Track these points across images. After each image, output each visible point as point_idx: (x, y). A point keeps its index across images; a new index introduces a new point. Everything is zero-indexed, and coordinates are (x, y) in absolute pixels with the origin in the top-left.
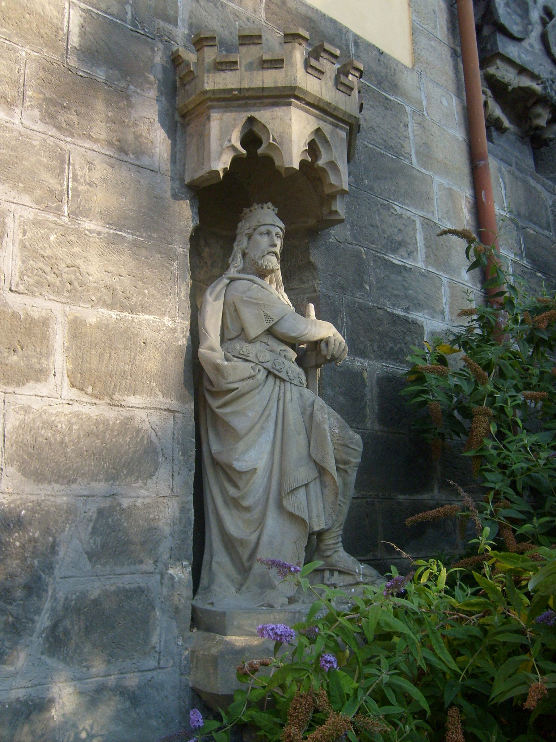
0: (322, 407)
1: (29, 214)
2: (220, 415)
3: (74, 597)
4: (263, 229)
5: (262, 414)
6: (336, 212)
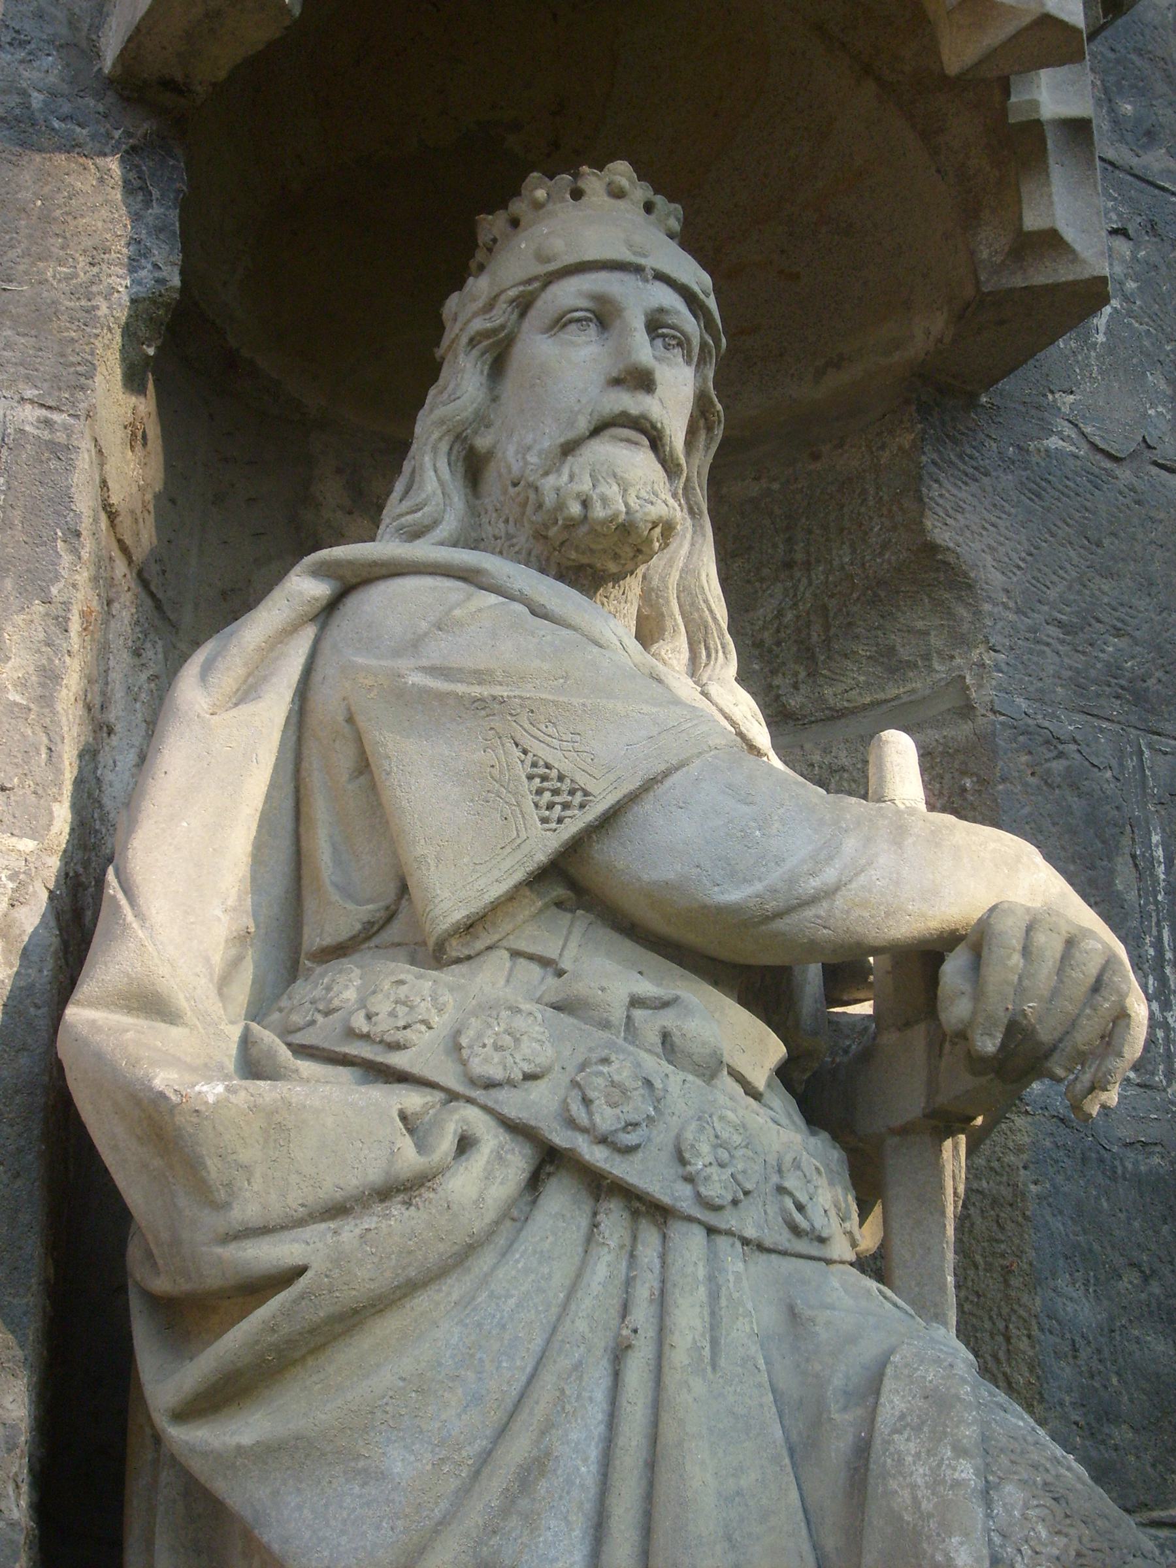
0: (939, 1402)
2: (197, 1466)
4: (569, 293)
5: (486, 1457)
6: (1052, 240)
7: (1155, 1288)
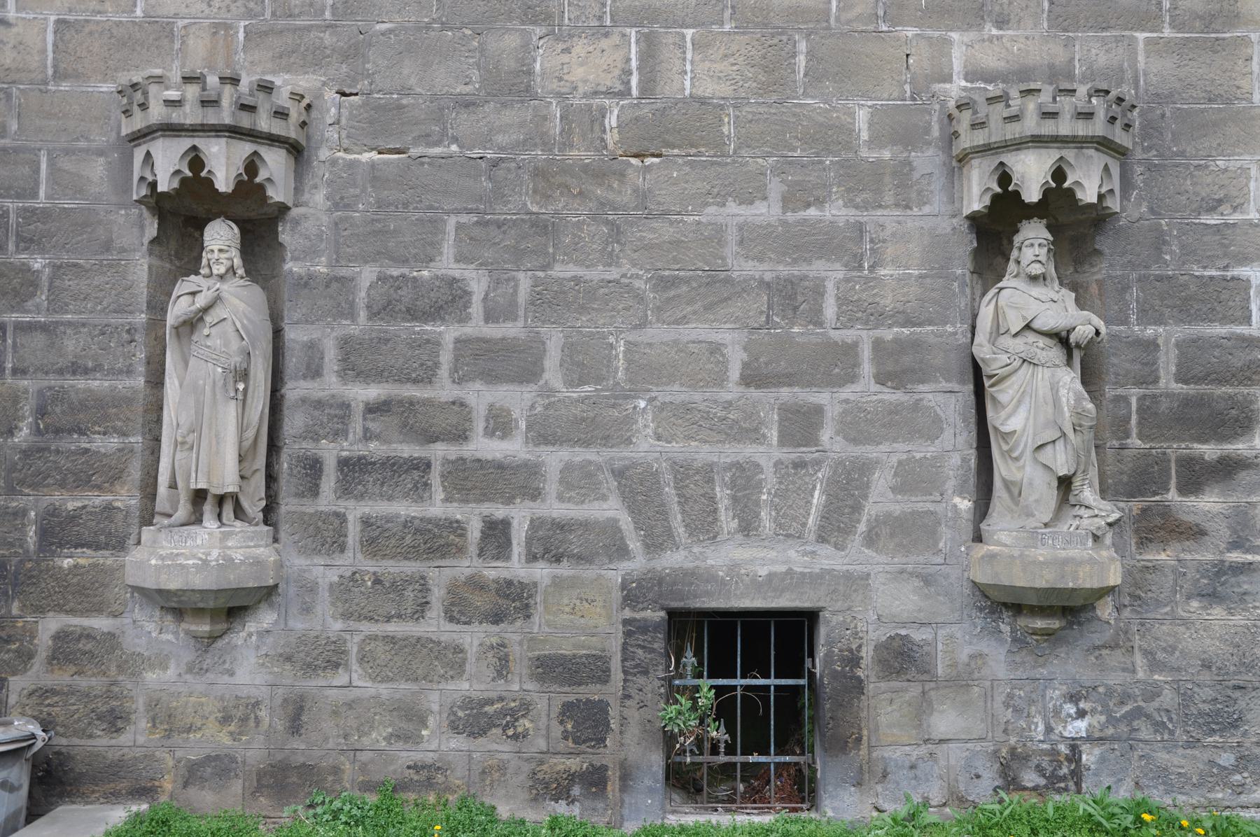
1: (840, 275)
4: (1027, 243)
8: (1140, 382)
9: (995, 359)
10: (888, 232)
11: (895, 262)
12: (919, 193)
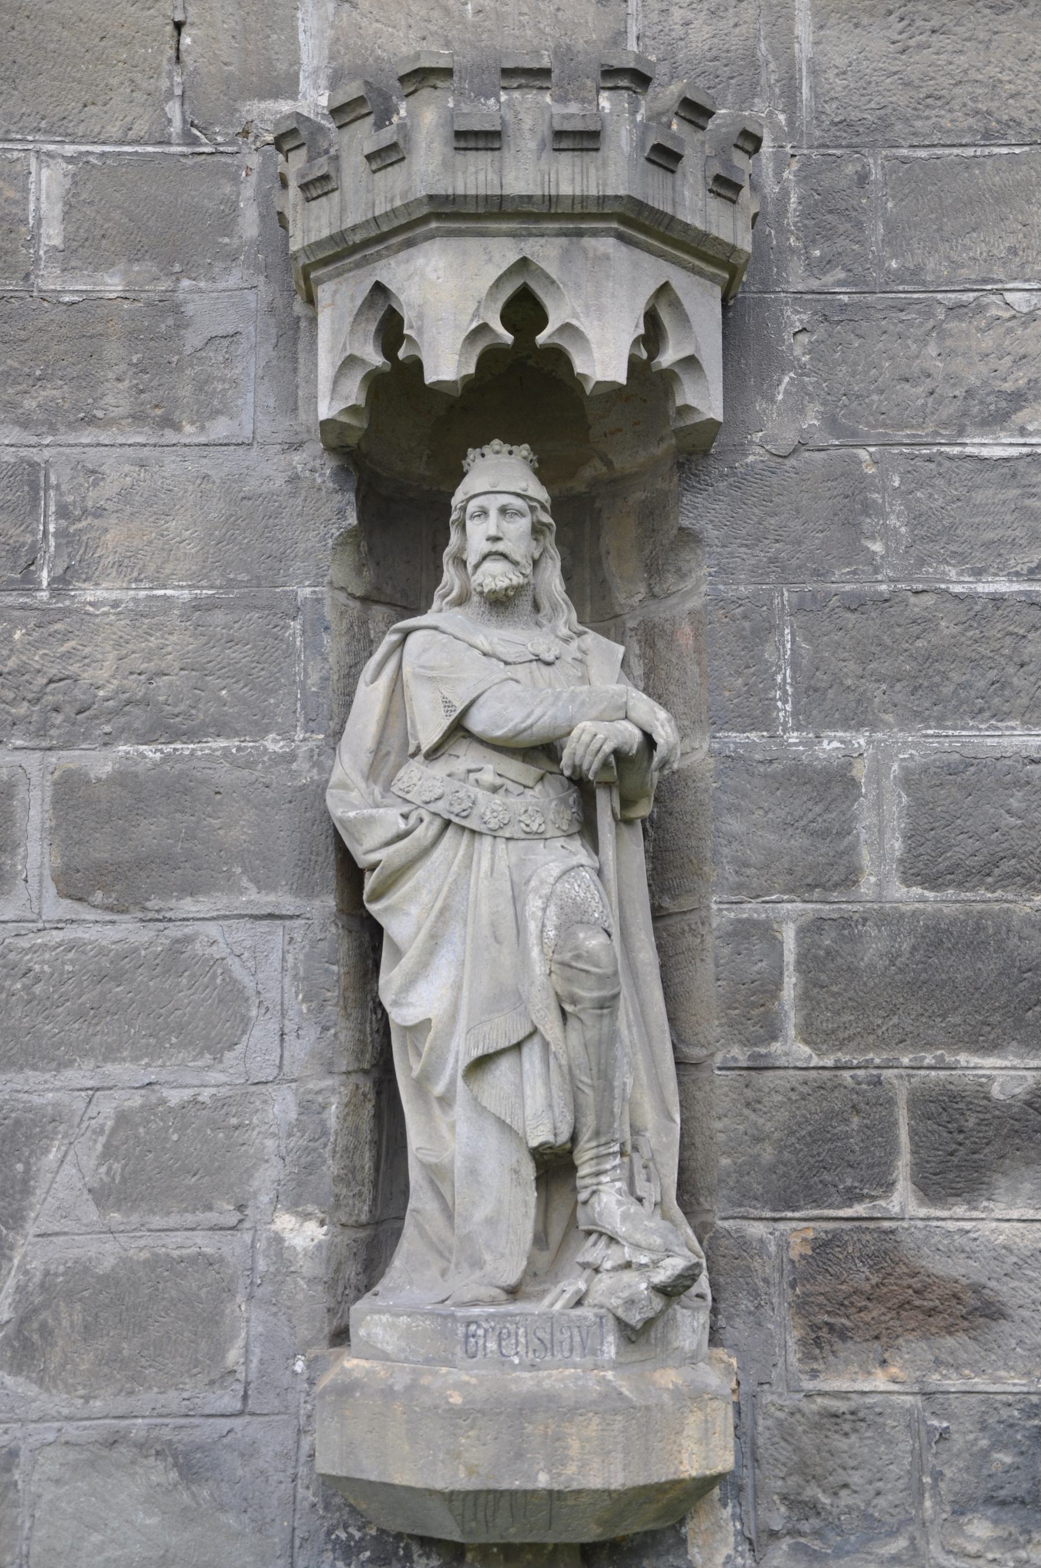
3: (61, 1269)
7: (770, 815)
8: (807, 884)
9: (369, 821)
10: (110, 488)
11: (126, 567)
12: (202, 385)
